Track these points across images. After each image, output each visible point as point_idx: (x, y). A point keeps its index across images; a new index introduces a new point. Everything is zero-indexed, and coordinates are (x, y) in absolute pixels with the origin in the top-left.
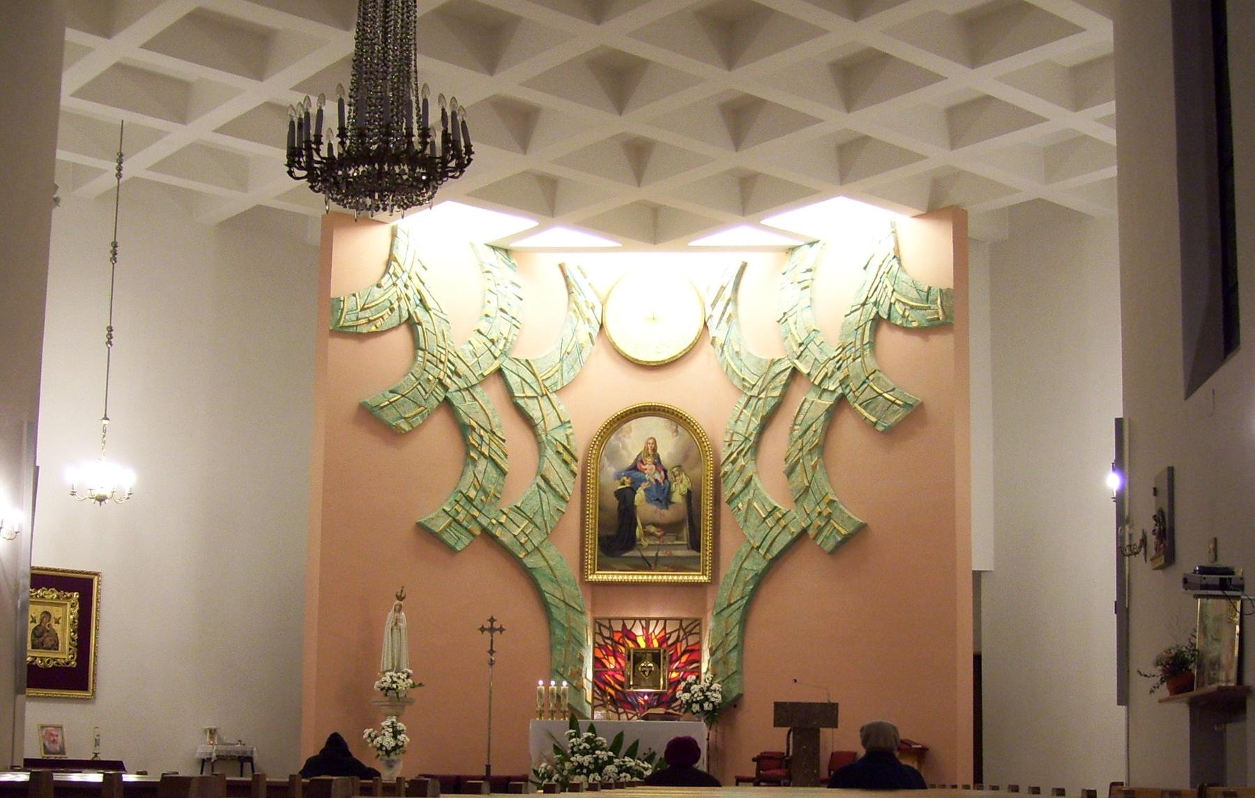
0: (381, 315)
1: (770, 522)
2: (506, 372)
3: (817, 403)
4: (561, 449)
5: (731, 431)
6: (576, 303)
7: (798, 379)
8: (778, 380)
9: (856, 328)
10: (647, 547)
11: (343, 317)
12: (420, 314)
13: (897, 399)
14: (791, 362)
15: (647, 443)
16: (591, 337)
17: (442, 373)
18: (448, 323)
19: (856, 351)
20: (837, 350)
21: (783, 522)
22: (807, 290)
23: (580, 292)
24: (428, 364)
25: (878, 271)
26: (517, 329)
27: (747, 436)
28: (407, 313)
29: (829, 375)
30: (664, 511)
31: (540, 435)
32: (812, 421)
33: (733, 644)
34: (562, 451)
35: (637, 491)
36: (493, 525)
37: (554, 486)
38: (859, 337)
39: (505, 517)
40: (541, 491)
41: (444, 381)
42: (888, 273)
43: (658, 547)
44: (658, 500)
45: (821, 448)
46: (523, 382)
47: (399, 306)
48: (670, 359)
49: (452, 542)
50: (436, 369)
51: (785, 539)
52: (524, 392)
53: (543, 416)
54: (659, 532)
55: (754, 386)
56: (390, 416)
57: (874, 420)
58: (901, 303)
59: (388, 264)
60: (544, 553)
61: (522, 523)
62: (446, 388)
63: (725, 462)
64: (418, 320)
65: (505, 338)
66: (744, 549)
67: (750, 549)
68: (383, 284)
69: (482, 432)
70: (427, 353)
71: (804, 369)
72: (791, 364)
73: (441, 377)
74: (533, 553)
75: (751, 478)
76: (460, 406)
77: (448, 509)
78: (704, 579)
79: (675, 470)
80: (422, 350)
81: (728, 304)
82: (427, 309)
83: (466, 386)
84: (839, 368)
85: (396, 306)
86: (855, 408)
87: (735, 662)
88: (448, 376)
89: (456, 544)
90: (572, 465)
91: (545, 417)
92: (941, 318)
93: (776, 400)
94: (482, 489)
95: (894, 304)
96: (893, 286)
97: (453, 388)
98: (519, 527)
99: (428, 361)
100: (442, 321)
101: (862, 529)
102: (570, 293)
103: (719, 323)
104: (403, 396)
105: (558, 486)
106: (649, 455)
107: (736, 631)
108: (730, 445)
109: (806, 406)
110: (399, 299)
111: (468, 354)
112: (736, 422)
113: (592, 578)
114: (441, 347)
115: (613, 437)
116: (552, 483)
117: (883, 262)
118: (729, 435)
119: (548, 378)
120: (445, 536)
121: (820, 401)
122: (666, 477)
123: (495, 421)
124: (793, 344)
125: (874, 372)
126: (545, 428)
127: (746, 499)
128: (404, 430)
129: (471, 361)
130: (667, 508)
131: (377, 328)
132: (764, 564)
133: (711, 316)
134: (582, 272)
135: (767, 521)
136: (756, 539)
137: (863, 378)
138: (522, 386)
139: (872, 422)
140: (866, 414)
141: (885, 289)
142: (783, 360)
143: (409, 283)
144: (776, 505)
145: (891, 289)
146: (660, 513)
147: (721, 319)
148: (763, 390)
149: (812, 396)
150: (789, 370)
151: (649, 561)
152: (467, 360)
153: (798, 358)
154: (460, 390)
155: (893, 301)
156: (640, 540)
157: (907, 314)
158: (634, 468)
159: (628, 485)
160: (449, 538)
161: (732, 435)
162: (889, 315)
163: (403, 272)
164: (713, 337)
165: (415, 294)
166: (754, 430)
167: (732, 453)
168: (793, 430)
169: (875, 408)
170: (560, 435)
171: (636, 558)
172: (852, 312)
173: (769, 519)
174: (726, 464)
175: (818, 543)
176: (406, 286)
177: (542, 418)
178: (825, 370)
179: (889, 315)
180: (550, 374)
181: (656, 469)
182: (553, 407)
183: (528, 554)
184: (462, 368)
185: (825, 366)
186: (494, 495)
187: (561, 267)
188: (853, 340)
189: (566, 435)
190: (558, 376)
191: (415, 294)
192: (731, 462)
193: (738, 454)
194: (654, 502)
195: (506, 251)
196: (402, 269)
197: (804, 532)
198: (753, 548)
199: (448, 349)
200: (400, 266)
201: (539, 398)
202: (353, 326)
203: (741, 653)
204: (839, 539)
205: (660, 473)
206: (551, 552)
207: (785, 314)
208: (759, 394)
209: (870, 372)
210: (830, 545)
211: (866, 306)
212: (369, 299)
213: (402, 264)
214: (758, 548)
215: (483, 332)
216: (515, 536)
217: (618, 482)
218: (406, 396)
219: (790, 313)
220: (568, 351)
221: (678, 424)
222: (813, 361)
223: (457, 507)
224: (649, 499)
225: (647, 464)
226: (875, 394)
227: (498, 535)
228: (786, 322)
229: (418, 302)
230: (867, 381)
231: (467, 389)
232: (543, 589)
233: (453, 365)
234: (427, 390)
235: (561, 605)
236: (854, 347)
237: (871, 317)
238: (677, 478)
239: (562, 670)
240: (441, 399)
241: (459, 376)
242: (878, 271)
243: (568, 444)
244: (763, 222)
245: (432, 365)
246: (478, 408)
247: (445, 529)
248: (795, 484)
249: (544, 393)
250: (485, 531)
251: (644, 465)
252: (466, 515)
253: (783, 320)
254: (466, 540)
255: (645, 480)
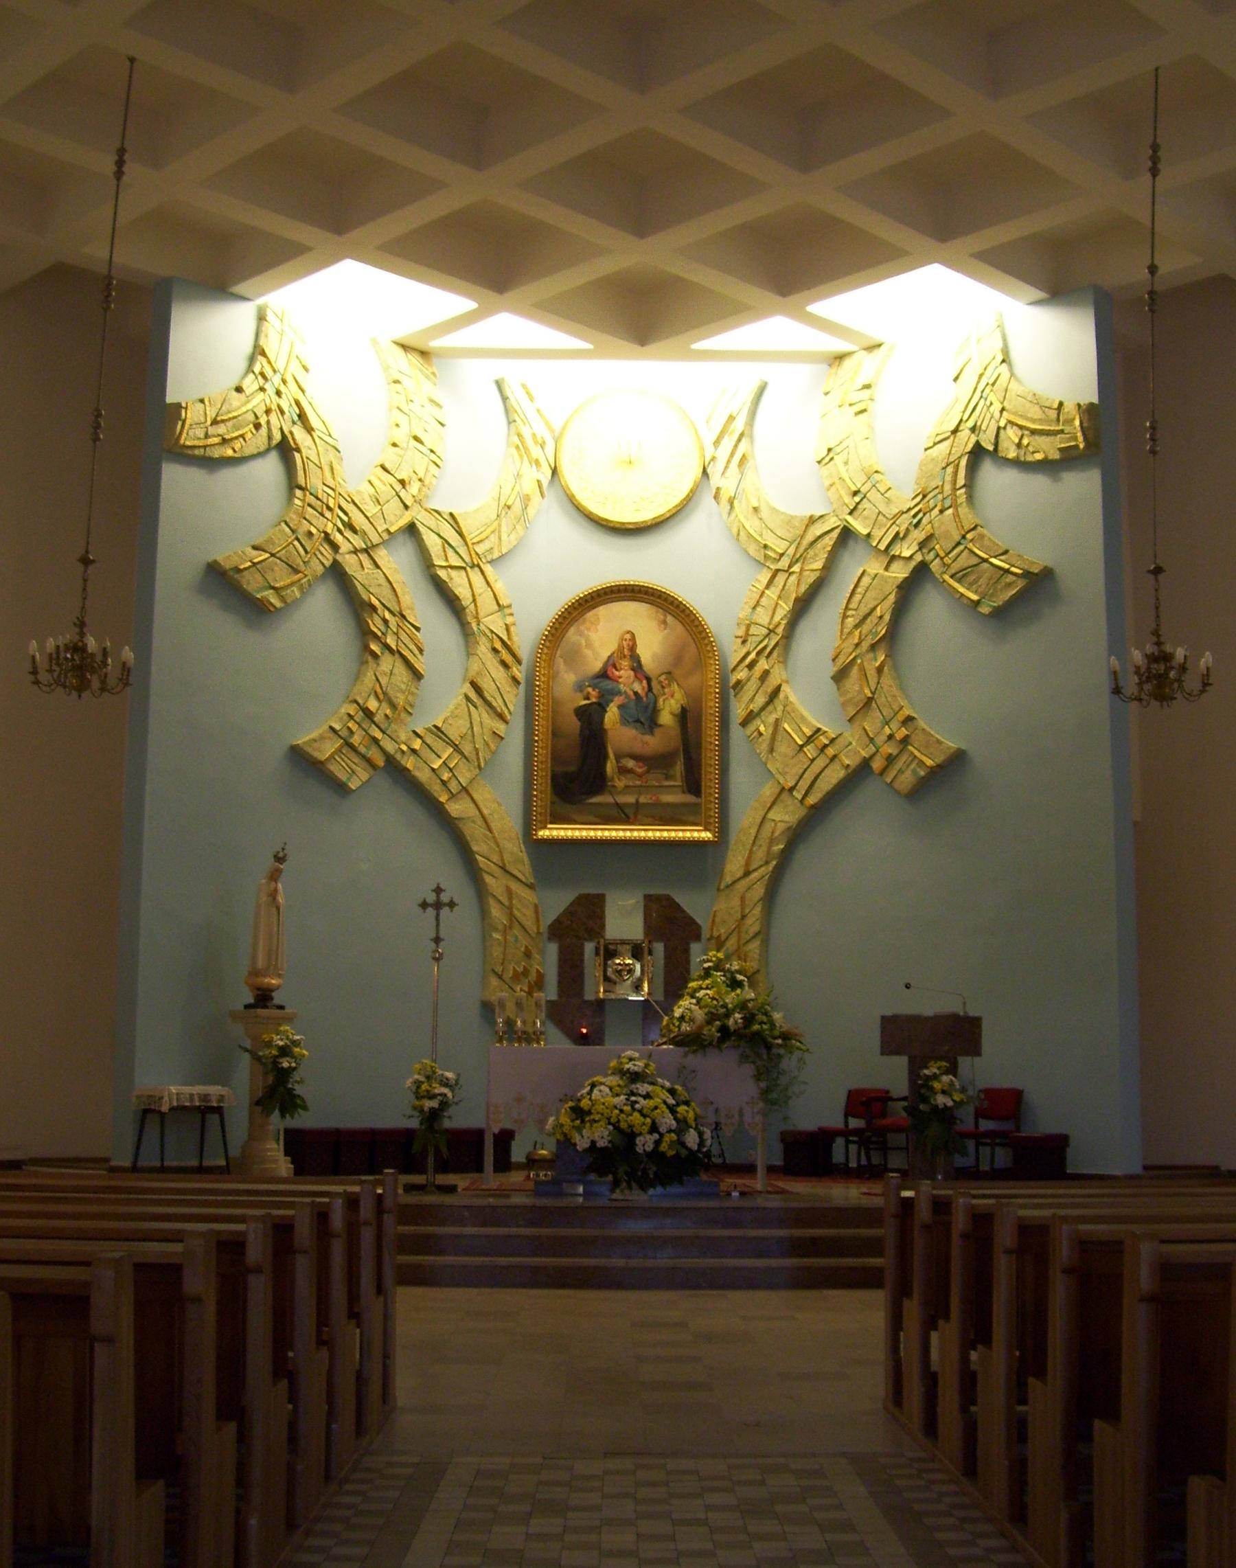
0: (240, 432)
1: (810, 751)
2: (422, 529)
3: (883, 576)
4: (498, 646)
5: (748, 622)
6: (519, 435)
7: (851, 543)
8: (819, 545)
9: (944, 465)
10: (622, 789)
11: (185, 431)
12: (299, 434)
13: (1013, 566)
14: (840, 520)
15: (622, 639)
16: (540, 486)
17: (330, 525)
18: (339, 452)
19: (944, 499)
20: (913, 499)
21: (831, 751)
22: (865, 414)
23: (525, 420)
24: (309, 509)
25: (978, 382)
26: (437, 468)
27: (771, 627)
28: (279, 433)
29: (901, 535)
30: (648, 738)
31: (469, 623)
32: (875, 603)
33: (756, 928)
34: (500, 649)
35: (608, 709)
36: (403, 752)
37: (489, 698)
38: (948, 478)
39: (419, 741)
40: (470, 705)
41: (332, 538)
42: (993, 385)
43: (639, 790)
44: (638, 721)
45: (892, 638)
46: (446, 545)
47: (268, 423)
48: (654, 519)
49: (343, 776)
50: (321, 518)
51: (834, 775)
52: (447, 560)
53: (473, 595)
54: (640, 767)
55: (782, 555)
56: (252, 583)
57: (975, 597)
58: (1015, 427)
59: (252, 360)
60: (475, 796)
61: (773, 593)
62: (335, 547)
63: (737, 665)
64: (295, 443)
65: (420, 480)
66: (769, 791)
67: (778, 790)
68: (244, 388)
69: (387, 615)
70: (308, 493)
71: (860, 527)
72: (839, 523)
73: (329, 531)
74: (459, 795)
75: (777, 690)
76: (354, 574)
77: (337, 727)
78: (707, 835)
79: (662, 678)
80: (300, 488)
81: (739, 440)
82: (309, 429)
83: (365, 547)
84: (917, 526)
85: (263, 420)
86: (944, 581)
87: (756, 956)
88: (339, 531)
89: (349, 779)
90: (514, 668)
91: (477, 597)
92: (1082, 446)
93: (818, 574)
94: (384, 697)
95: (1005, 428)
96: (1002, 403)
97: (345, 547)
98: (439, 757)
99: (309, 505)
100: (329, 448)
101: (958, 759)
102: (510, 422)
103: (726, 467)
104: (273, 555)
105: (494, 698)
106: (625, 656)
107: (757, 911)
108: (744, 642)
109: (866, 581)
110: (268, 412)
111: (368, 500)
112: (754, 608)
113: (544, 833)
114: (328, 487)
115: (572, 630)
116: (486, 694)
117: (985, 369)
118: (743, 628)
119: (481, 541)
120: (333, 768)
121: (886, 573)
122: (650, 689)
123: (406, 599)
124: (843, 493)
125: (974, 528)
126: (477, 613)
127: (771, 719)
128: (275, 607)
129: (372, 510)
130: (652, 733)
131: (234, 451)
132: (801, 812)
133: (713, 459)
134: (527, 393)
135: (805, 749)
136: (788, 777)
137: (957, 538)
138: (445, 551)
139: (972, 601)
140: (962, 590)
141: (989, 407)
142: (827, 518)
143: (282, 388)
144: (819, 726)
145: (997, 407)
146: (642, 741)
147: (729, 462)
148: (797, 561)
149: (875, 567)
150: (837, 531)
151: (627, 811)
152: (366, 507)
153: (851, 513)
154: (355, 551)
155: (1002, 424)
156: (612, 780)
157: (1025, 442)
158: (604, 675)
159: (594, 700)
160: (338, 770)
161: (748, 627)
162: (996, 445)
163: (275, 371)
164: (718, 489)
165: (291, 405)
166: (782, 619)
167: (748, 654)
168: (845, 617)
169: (975, 581)
170: (495, 623)
171: (608, 805)
172: (935, 444)
173: (808, 747)
174: (740, 668)
175: (889, 780)
176: (278, 393)
177: (471, 599)
178: (894, 530)
179: (996, 445)
180: (482, 536)
181: (636, 676)
182: (488, 583)
183: (453, 796)
184: (359, 520)
185: (894, 523)
186: (404, 708)
187: (499, 384)
188: (941, 483)
189: (506, 625)
190: (494, 538)
191: (291, 405)
192: (747, 666)
193: (759, 654)
194: (633, 724)
195: (424, 354)
196: (272, 366)
197: (865, 764)
198: (783, 789)
199: (339, 490)
200: (269, 362)
201: (468, 569)
202: (199, 447)
203: (766, 942)
204: (922, 773)
205: (641, 682)
206: (483, 794)
207: (829, 450)
208: (790, 566)
209: (967, 528)
210: (906, 780)
211: (959, 434)
212: (223, 408)
213: (272, 360)
214: (792, 789)
215: (389, 469)
216: (433, 770)
217: (579, 695)
218: (278, 555)
219: (838, 450)
220: (509, 503)
221: (666, 611)
222: (875, 517)
223: (351, 724)
224: (625, 720)
225: (621, 669)
226: (975, 561)
227: (411, 768)
228: (832, 462)
229: (296, 418)
230: (962, 541)
231: (366, 551)
232: (475, 848)
233: (346, 513)
234: (309, 550)
235: (498, 871)
236: (942, 493)
237: (969, 448)
238: (666, 690)
239: (501, 969)
240: (327, 564)
241: (355, 531)
242: (978, 382)
243: (509, 638)
244: (810, 308)
245: (315, 512)
246: (382, 581)
247: (332, 757)
248: (849, 696)
249: (476, 563)
250: (389, 759)
251: (617, 670)
252: (364, 737)
253: (827, 459)
254: (363, 774)
255: (619, 693)
